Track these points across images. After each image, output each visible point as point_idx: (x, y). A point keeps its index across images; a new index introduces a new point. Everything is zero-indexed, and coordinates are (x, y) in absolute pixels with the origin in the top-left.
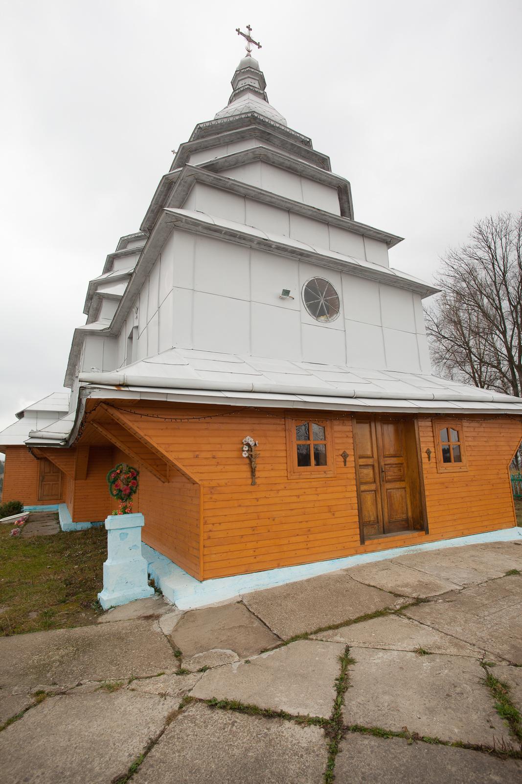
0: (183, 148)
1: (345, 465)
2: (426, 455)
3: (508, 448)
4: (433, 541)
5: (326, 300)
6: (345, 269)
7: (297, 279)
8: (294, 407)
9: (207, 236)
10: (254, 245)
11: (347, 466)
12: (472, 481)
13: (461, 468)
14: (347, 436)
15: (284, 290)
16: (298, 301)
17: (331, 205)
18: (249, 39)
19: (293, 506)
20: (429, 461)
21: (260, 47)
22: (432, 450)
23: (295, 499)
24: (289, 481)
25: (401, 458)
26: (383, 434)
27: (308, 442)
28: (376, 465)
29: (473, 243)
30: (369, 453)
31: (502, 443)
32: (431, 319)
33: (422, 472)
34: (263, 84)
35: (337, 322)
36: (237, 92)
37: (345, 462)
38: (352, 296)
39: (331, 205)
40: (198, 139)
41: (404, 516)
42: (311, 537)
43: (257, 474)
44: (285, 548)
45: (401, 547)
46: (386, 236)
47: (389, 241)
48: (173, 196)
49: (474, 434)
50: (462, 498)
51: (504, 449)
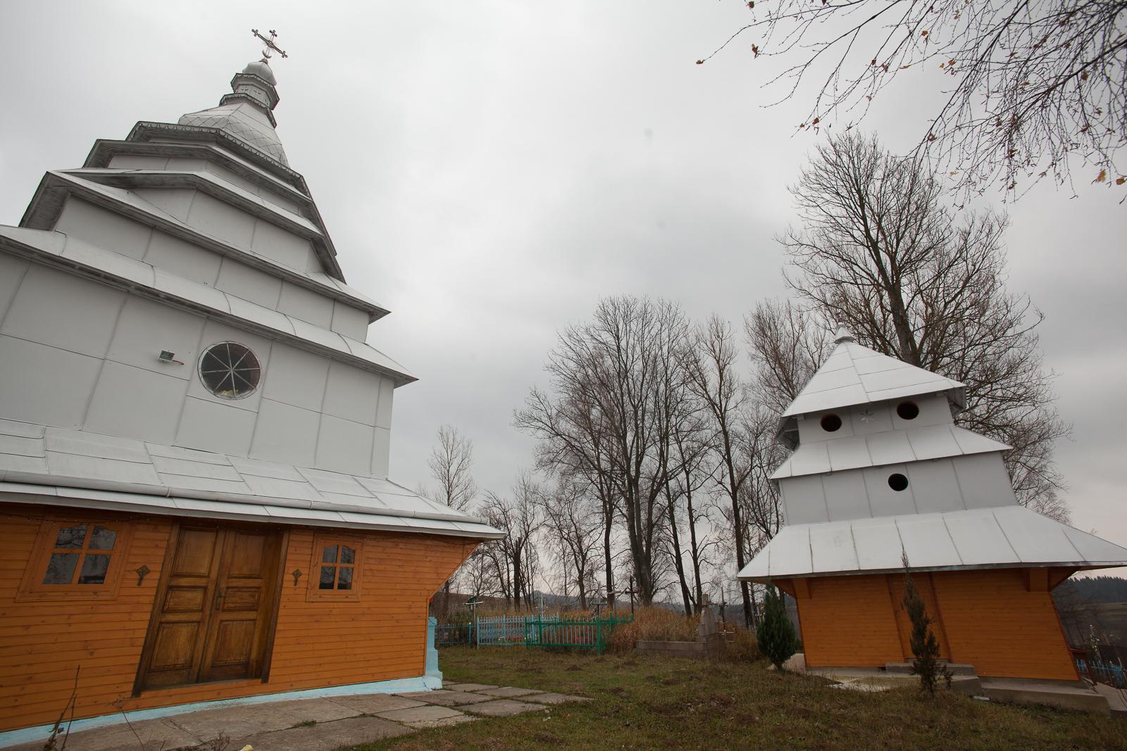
0: (102, 145)
1: (139, 584)
4: (272, 692)
5: (239, 373)
6: (278, 338)
8: (36, 502)
9: (48, 267)
10: (132, 289)
11: (143, 585)
12: (363, 614)
13: (347, 597)
14: (157, 546)
15: (163, 352)
17: (298, 261)
18: (270, 44)
20: (295, 585)
21: (284, 55)
22: (304, 571)
24: (16, 605)
25: (260, 580)
28: (211, 588)
29: (598, 324)
30: (204, 571)
33: (279, 600)
34: (275, 100)
35: (249, 400)
36: (236, 96)
37: (296, 581)
38: (277, 373)
39: (298, 261)
40: (139, 140)
41: (243, 659)
46: (365, 305)
48: (39, 203)
50: (341, 636)
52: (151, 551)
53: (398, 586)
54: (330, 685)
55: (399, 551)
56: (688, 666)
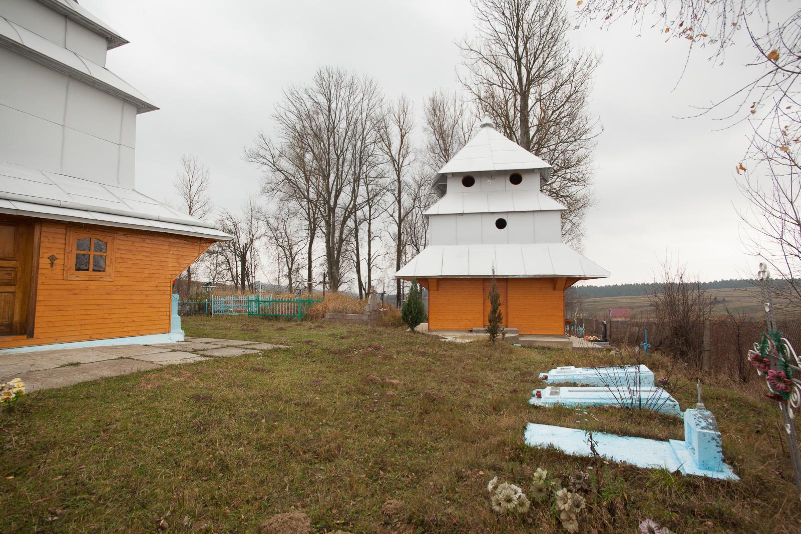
3: (176, 265)
27: (89, 253)
29: (316, 87)
31: (169, 260)
32: (268, 149)
47: (112, 40)
51: (171, 264)
53: (146, 271)
54: (91, 339)
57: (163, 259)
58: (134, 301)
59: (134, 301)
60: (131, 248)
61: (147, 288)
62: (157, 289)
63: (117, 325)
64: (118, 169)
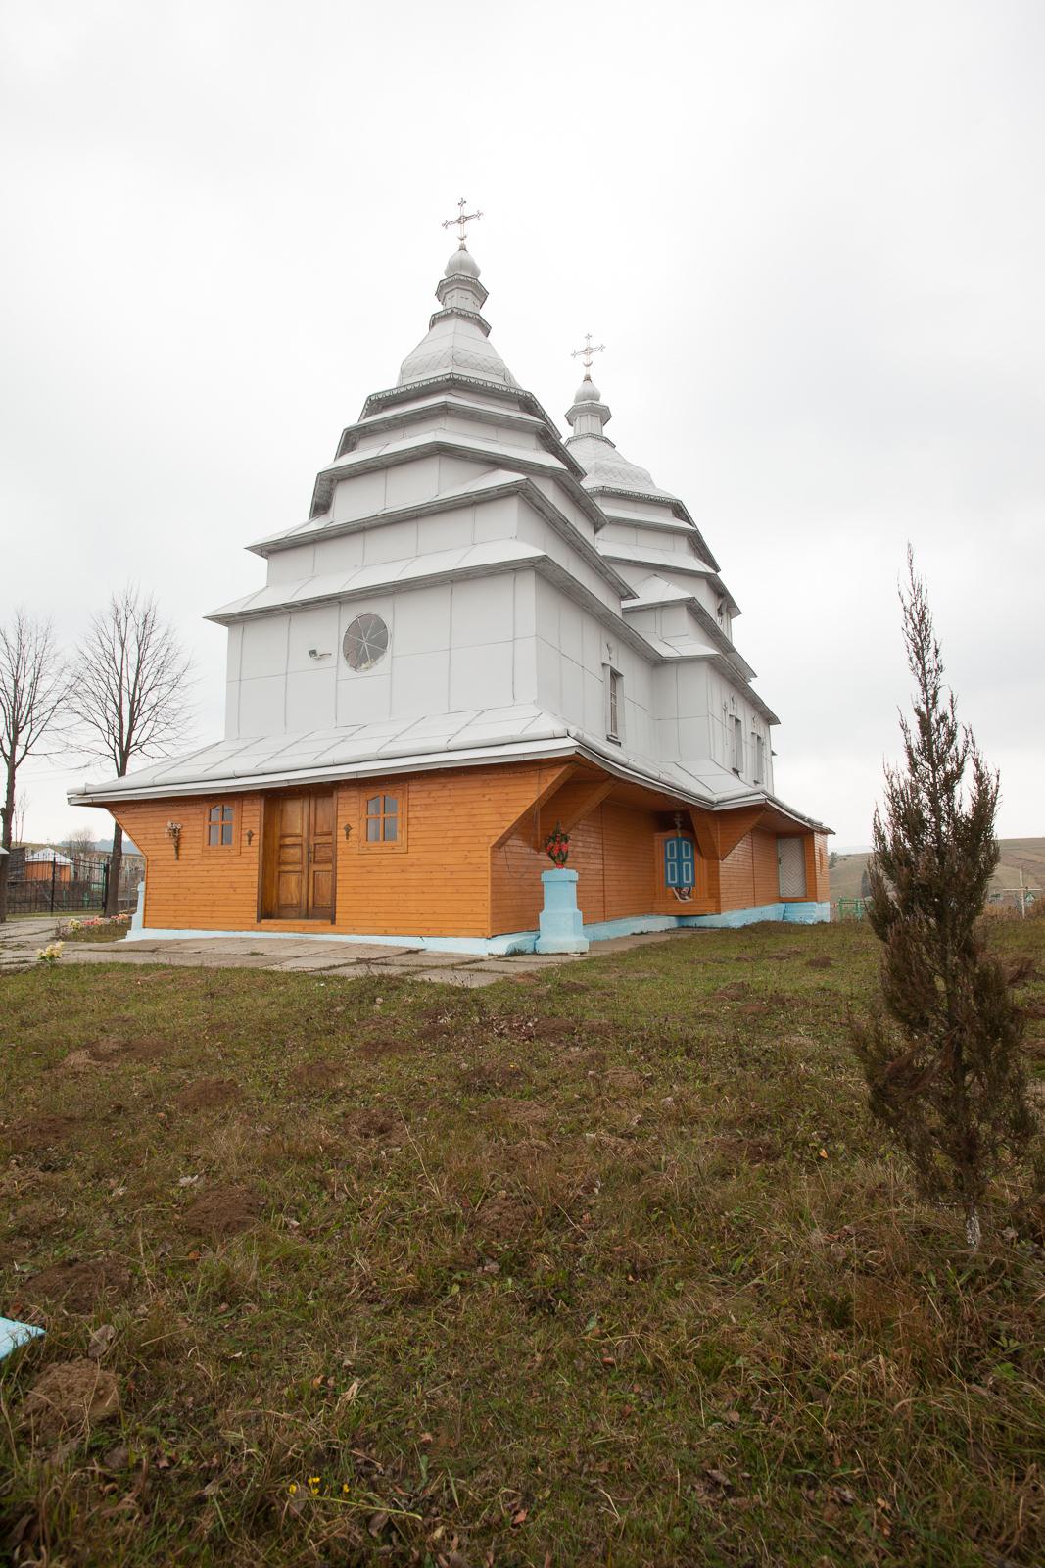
2: (247, 838)
7: (329, 632)
16: (337, 660)
19: (205, 880)
23: (205, 873)
26: (316, 809)
28: (305, 844)
30: (298, 831)
31: (484, 811)
37: (250, 840)
42: (215, 908)
43: (181, 851)
44: (195, 914)
45: (299, 932)
49: (427, 801)
51: (486, 819)
52: (612, 782)
53: (449, 834)
54: (386, 934)
55: (446, 793)
56: (1000, 1137)
57: (475, 812)
58: (435, 882)
59: (435, 882)
60: (427, 801)
61: (451, 861)
62: (468, 861)
63: (414, 917)
64: (449, 688)
